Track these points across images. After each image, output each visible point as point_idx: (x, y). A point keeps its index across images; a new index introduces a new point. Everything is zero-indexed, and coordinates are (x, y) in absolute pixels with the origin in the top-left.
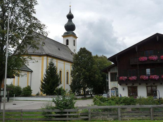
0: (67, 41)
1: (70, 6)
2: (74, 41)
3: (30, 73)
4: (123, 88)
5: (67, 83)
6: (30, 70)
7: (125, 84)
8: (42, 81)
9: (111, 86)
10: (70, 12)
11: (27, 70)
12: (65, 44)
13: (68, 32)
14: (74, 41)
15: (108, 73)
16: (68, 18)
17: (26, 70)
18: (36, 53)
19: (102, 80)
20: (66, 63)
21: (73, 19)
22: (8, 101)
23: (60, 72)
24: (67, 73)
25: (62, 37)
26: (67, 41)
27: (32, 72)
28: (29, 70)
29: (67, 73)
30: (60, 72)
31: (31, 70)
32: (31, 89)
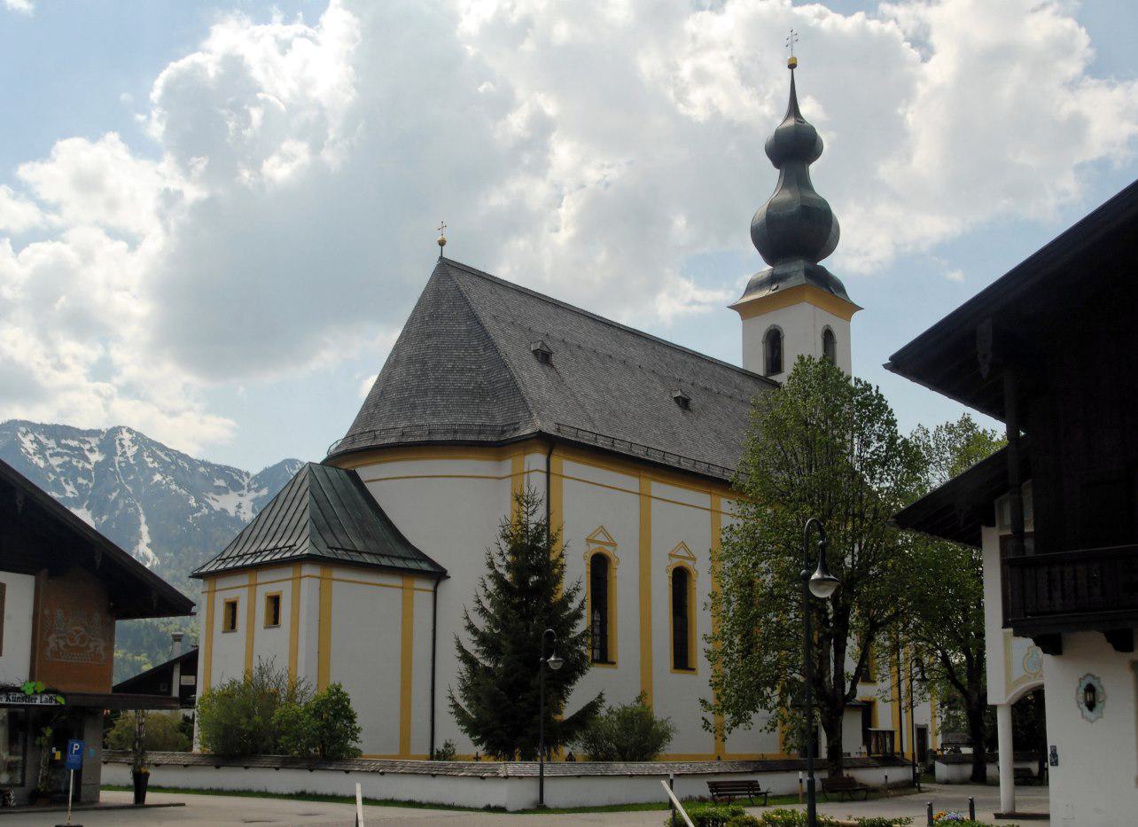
0: (774, 340)
1: (792, 66)
2: (828, 337)
3: (429, 586)
4: (1090, 689)
5: (682, 660)
6: (425, 566)
7: (1097, 638)
8: (471, 647)
9: (1008, 664)
10: (794, 108)
11: (399, 564)
12: (759, 368)
13: (779, 270)
14: (828, 337)
15: (977, 543)
16: (777, 164)
17: (385, 562)
18: (465, 432)
19: (764, 581)
20: (660, 489)
21: (814, 169)
22: (140, 798)
23: (600, 566)
24: (681, 579)
25: (736, 315)
26: (774, 340)
27: (437, 575)
28: (412, 565)
29: (681, 579)
30: (600, 566)
31: (423, 558)
32: (353, 706)
